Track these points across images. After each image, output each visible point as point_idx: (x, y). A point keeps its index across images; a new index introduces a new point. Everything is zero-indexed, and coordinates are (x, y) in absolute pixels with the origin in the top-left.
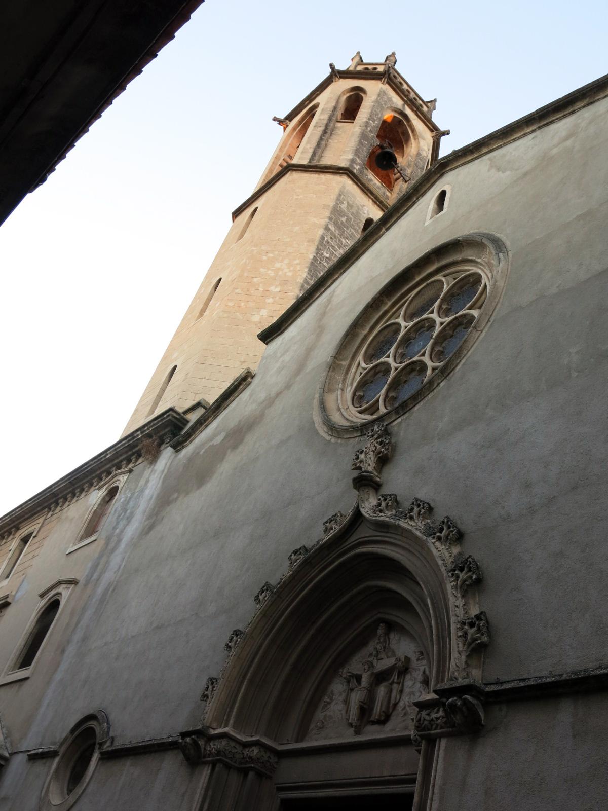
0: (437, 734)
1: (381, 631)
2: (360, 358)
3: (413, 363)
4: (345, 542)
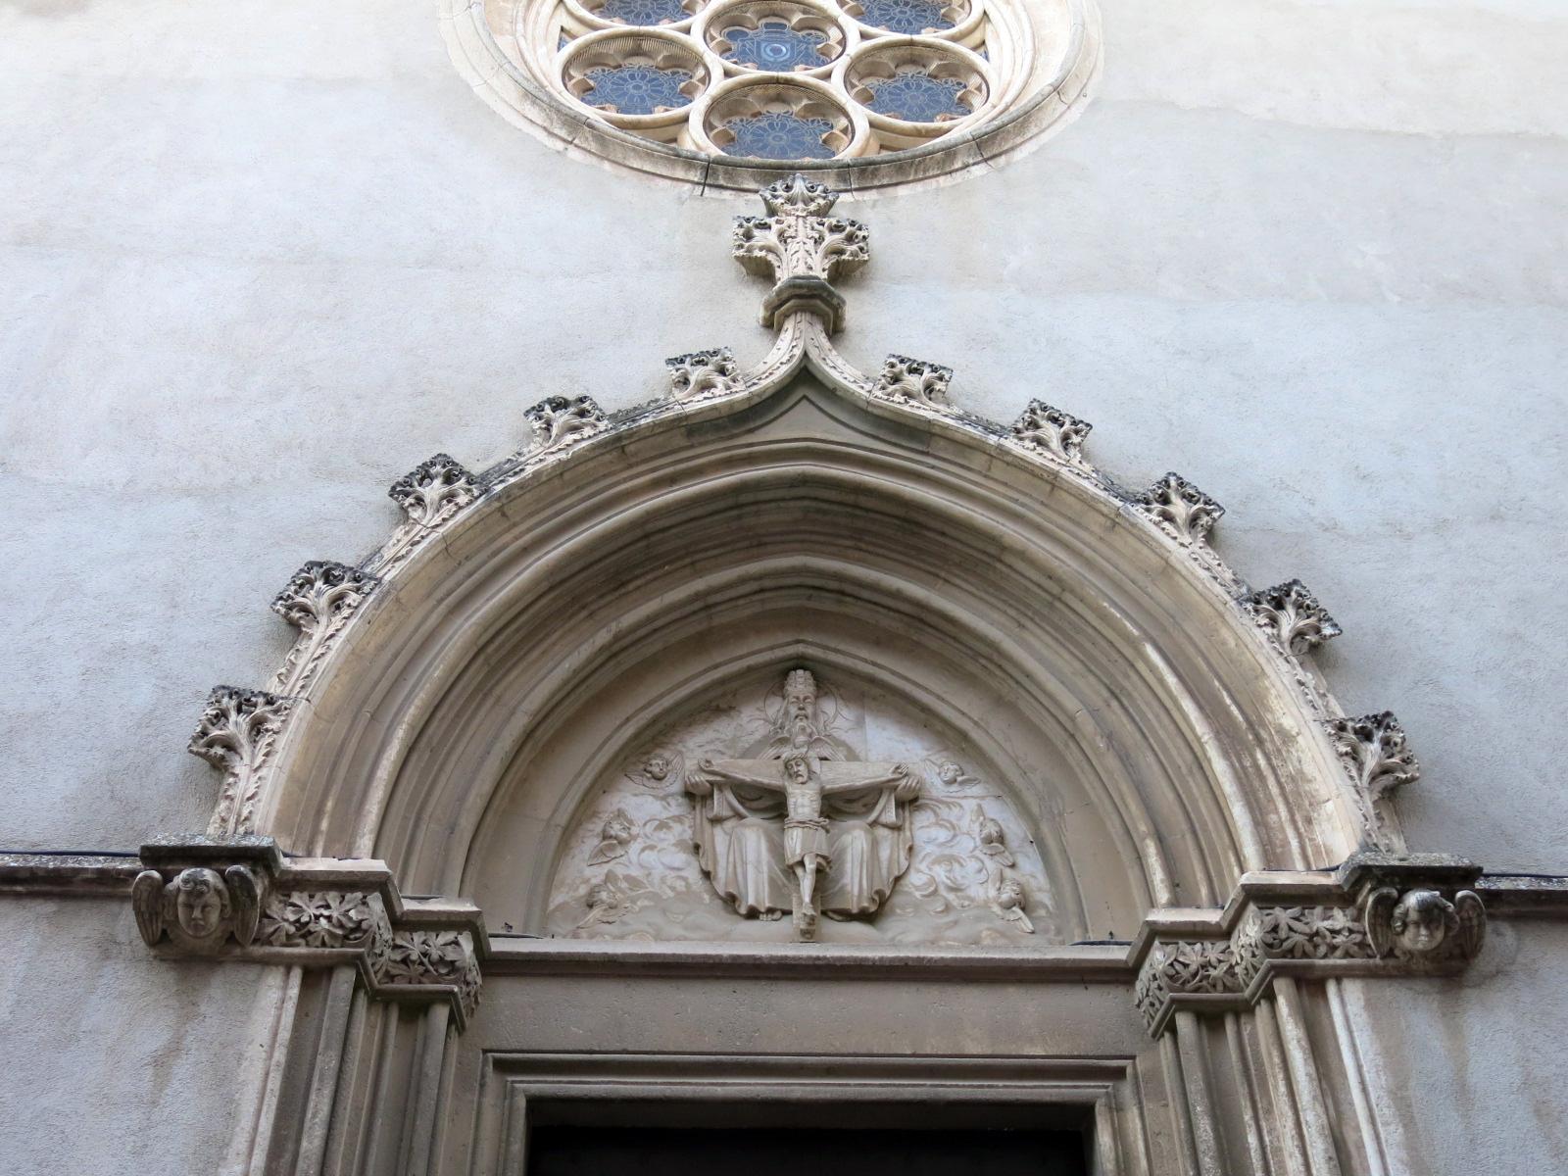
0: (1334, 967)
1: (800, 683)
3: (788, 82)
4: (751, 431)
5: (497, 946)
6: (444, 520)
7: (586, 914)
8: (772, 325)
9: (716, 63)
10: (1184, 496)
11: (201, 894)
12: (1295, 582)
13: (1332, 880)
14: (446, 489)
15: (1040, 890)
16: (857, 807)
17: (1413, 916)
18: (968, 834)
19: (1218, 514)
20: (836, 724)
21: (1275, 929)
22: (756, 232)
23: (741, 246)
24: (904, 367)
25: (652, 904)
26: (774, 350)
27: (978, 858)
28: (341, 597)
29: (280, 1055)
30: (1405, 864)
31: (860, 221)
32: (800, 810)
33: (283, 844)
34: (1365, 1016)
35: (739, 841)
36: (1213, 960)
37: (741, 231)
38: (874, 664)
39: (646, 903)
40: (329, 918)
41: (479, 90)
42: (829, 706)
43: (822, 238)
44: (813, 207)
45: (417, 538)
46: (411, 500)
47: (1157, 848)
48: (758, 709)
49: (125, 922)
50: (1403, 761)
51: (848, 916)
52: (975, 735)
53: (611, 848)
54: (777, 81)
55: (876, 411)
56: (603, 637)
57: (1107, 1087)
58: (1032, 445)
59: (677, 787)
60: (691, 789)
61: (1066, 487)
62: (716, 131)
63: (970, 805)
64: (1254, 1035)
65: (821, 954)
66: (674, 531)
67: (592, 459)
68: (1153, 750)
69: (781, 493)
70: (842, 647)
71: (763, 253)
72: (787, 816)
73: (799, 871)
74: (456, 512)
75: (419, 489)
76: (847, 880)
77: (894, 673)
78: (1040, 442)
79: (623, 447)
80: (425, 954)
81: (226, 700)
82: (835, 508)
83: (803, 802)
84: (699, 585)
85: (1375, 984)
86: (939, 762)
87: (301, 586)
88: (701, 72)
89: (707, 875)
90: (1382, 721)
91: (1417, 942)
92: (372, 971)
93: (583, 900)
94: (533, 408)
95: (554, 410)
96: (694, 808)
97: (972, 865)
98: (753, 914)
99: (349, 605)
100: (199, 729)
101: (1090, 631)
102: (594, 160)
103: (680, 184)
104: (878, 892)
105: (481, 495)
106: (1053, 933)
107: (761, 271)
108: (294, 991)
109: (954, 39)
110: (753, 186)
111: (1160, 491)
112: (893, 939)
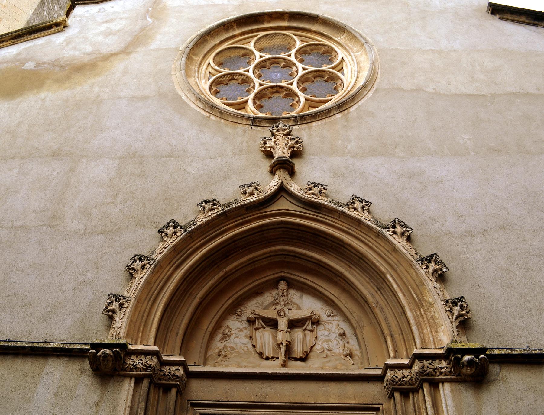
0: (441, 379)
1: (283, 285)
2: (210, 59)
3: (280, 86)
4: (266, 208)
5: (191, 369)
6: (174, 240)
7: (217, 358)
8: (273, 172)
9: (257, 81)
10: (400, 225)
11: (106, 357)
12: (435, 254)
13: (442, 351)
14: (174, 230)
15: (356, 350)
16: (299, 324)
17: (465, 363)
18: (334, 332)
19: (411, 231)
20: (294, 297)
21: (423, 367)
22: (268, 142)
23: (263, 147)
24: (313, 185)
25: (237, 355)
26: (273, 181)
27: (337, 340)
28: (144, 265)
29: (129, 403)
30: (464, 347)
31: (300, 137)
32: (281, 326)
33: (129, 341)
34: (450, 394)
35: (264, 335)
36: (406, 375)
37: (263, 142)
38: (305, 279)
39: (236, 355)
40: (142, 364)
41: (184, 98)
42: (291, 292)
43: (288, 143)
44: (285, 132)
45: (166, 247)
46: (164, 234)
47: (390, 339)
48: (270, 293)
49: (87, 365)
50: (467, 312)
51: (296, 359)
52: (336, 301)
53: (225, 338)
54: (276, 86)
55: (304, 200)
56: (221, 273)
57: (374, 413)
58: (352, 210)
59: (245, 318)
60: (249, 319)
61: (363, 223)
62: (257, 104)
63: (335, 323)
64: (418, 399)
65: (287, 372)
66: (243, 239)
67: (217, 219)
68: (390, 307)
69: (275, 226)
70: (295, 273)
71: (269, 149)
72: (278, 328)
73: (281, 346)
74: (177, 238)
75: (166, 231)
76: (296, 348)
77: (311, 281)
78: (355, 209)
79: (227, 215)
80: (170, 373)
81: (112, 298)
82: (292, 230)
83: (282, 324)
84: (251, 256)
85: (454, 384)
86: (325, 310)
87: (133, 262)
88: (252, 85)
89: (254, 346)
90: (461, 299)
91: (467, 372)
92: (154, 378)
93: (217, 354)
94: (200, 204)
95: (206, 204)
96: (250, 325)
97: (335, 342)
98: (267, 358)
99: (146, 268)
100: (105, 307)
101: (371, 269)
102: (218, 119)
103: (245, 125)
104: (305, 352)
105: (184, 232)
106: (360, 364)
107: (269, 155)
108: (133, 385)
109: (332, 68)
110: (267, 125)
111: (393, 224)
112: (310, 366)
